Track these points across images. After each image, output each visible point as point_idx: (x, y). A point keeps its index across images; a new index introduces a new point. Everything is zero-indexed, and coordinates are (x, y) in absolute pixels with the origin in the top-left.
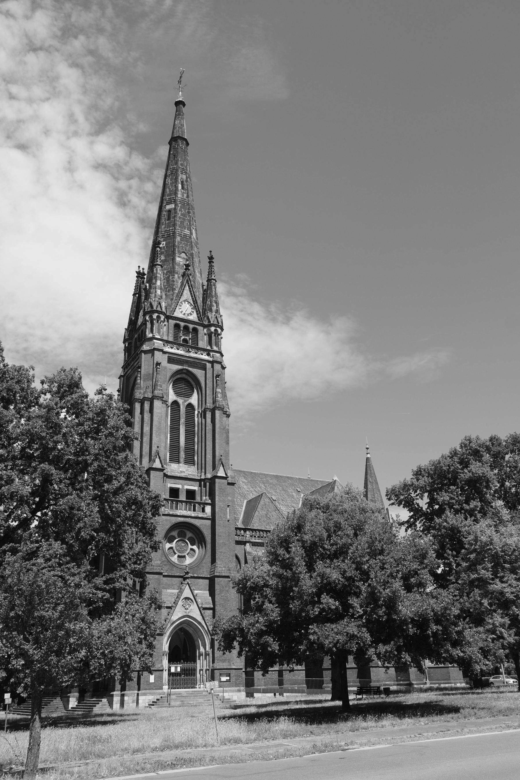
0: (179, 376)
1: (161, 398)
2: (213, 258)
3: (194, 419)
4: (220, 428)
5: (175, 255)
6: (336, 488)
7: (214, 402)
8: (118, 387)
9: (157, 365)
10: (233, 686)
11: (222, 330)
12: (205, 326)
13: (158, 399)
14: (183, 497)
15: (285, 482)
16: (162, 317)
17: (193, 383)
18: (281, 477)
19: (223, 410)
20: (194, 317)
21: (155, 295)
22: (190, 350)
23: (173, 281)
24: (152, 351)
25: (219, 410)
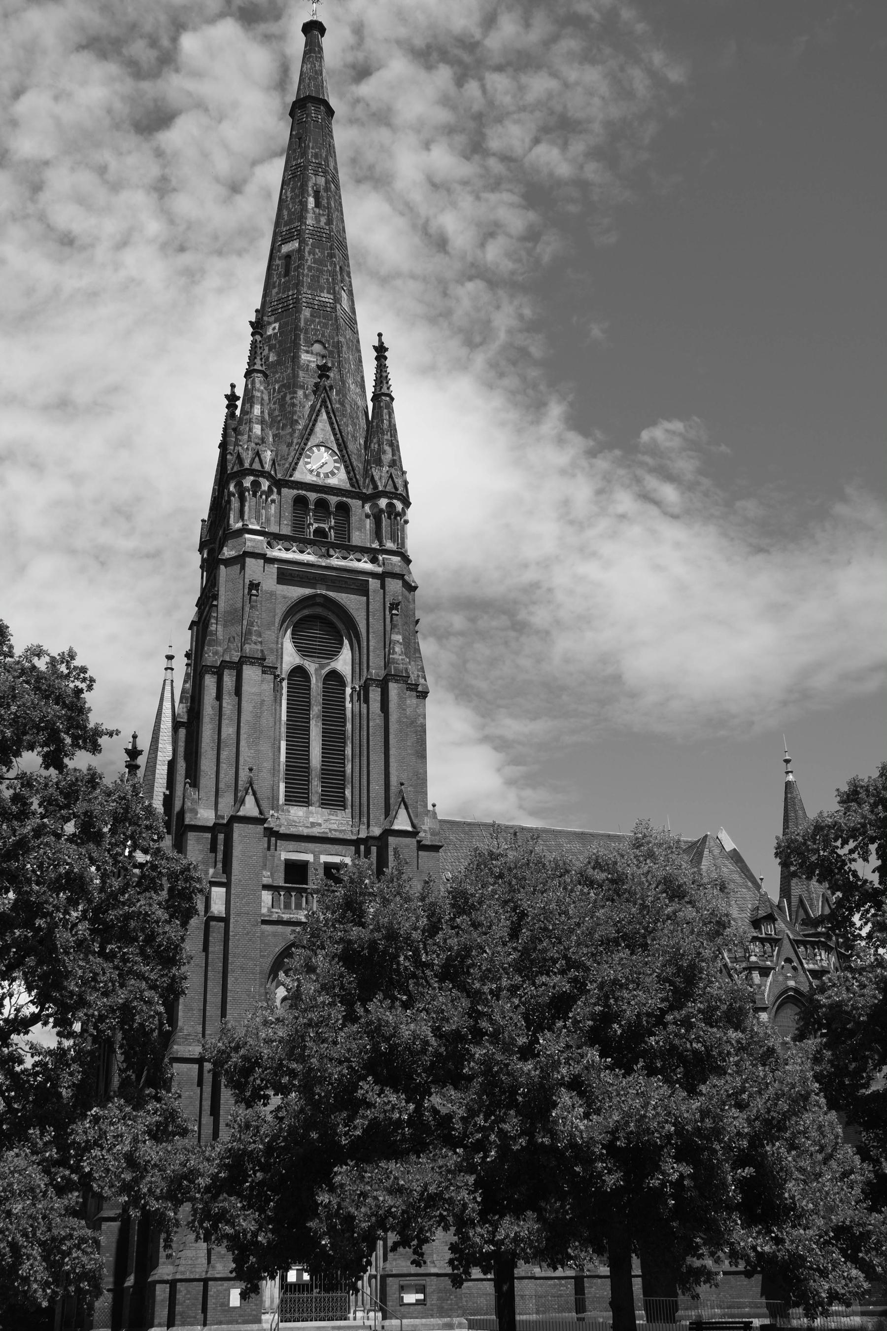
0: (306, 612)
1: (259, 661)
2: (386, 350)
3: (344, 706)
4: (399, 721)
5: (299, 349)
6: (706, 852)
7: (386, 665)
8: (189, 648)
9: (250, 590)
10: (432, 1316)
11: (407, 503)
12: (365, 499)
13: (252, 664)
14: (315, 880)
16: (265, 484)
17: (340, 626)
18: (592, 835)
19: (406, 682)
20: (340, 479)
21: (249, 436)
22: (332, 552)
23: (294, 405)
24: (240, 560)
25: (397, 681)
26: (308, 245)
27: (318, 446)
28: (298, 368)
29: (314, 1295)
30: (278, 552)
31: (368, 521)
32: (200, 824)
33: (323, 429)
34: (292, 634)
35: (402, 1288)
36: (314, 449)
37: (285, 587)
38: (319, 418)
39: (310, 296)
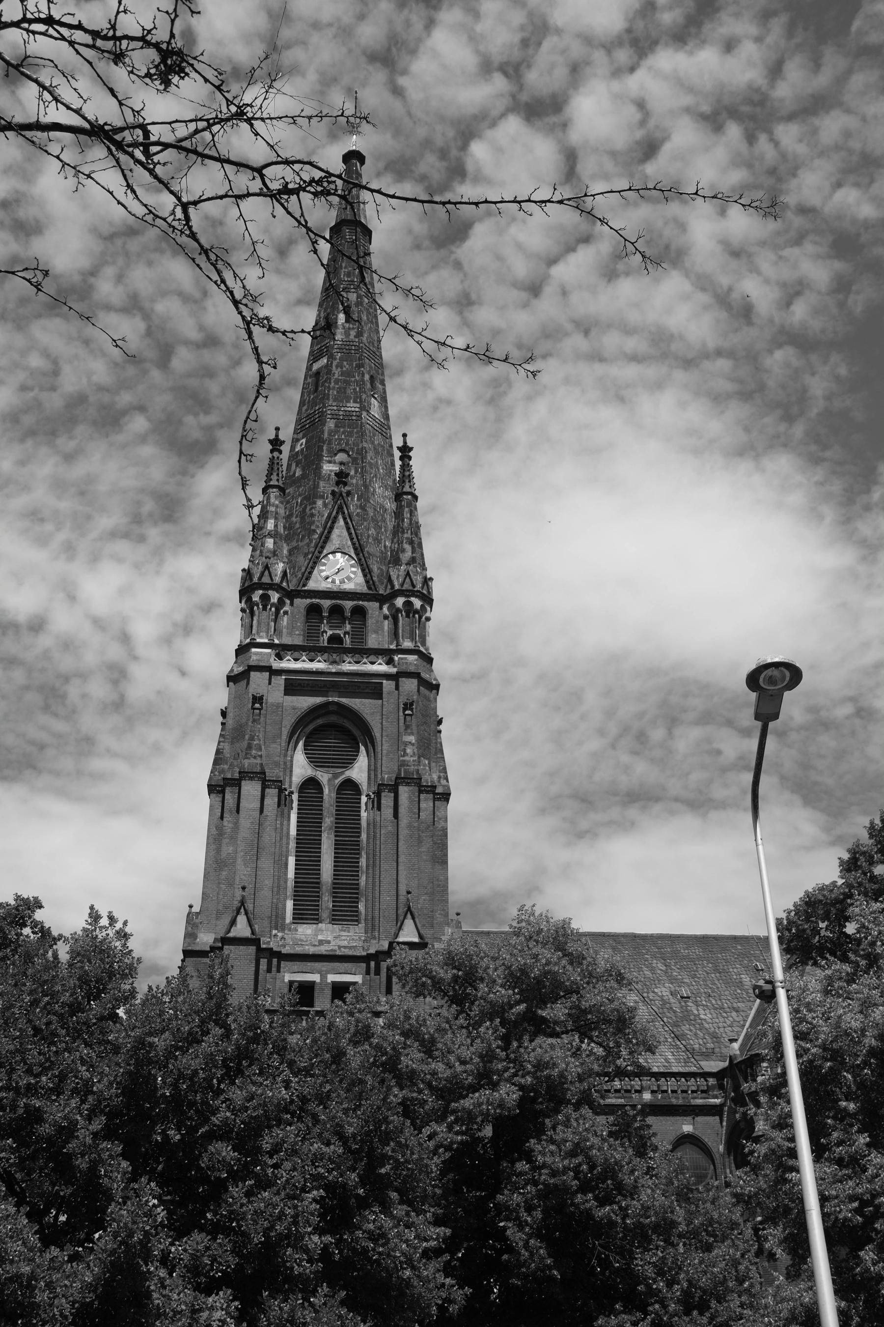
0: (320, 722)
2: (411, 449)
3: (359, 816)
4: (410, 826)
11: (428, 600)
12: (382, 600)
13: (251, 779)
15: (724, 950)
21: (261, 552)
23: (312, 515)
25: (407, 784)
26: (335, 359)
27: (333, 553)
28: (319, 478)
31: (386, 622)
32: (197, 948)
33: (339, 533)
34: (305, 745)
37: (294, 698)
38: (336, 525)
39: (335, 408)
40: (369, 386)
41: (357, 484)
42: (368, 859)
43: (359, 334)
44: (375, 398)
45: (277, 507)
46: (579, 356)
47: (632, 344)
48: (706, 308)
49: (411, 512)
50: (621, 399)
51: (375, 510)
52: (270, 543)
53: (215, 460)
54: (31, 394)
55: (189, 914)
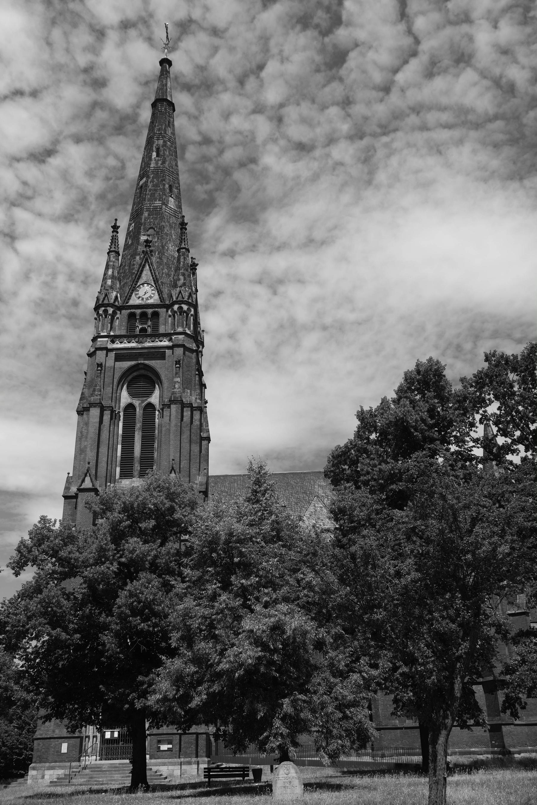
0: (135, 374)
12: (168, 307)
13: (95, 407)
16: (110, 310)
17: (154, 378)
20: (155, 299)
25: (175, 404)
29: (120, 745)
30: (118, 345)
31: (170, 318)
32: (70, 495)
33: (146, 274)
35: (159, 742)
36: (141, 286)
37: (121, 363)
40: (168, 191)
41: (158, 246)
42: (158, 443)
43: (164, 162)
44: (172, 197)
45: (114, 262)
46: (413, 129)
47: (445, 117)
48: (488, 89)
49: (184, 258)
50: (440, 152)
51: (168, 258)
52: (109, 282)
53: (216, 210)
54: (111, 182)
55: (68, 477)
